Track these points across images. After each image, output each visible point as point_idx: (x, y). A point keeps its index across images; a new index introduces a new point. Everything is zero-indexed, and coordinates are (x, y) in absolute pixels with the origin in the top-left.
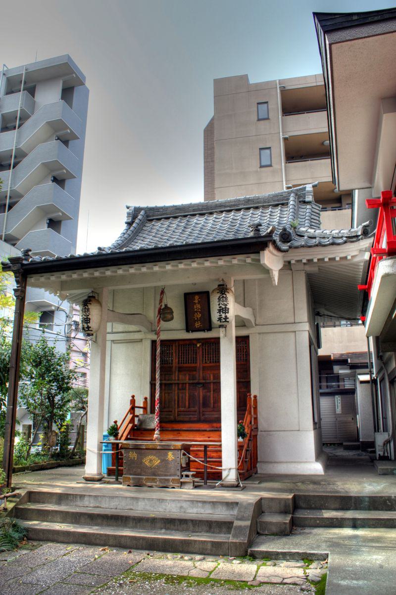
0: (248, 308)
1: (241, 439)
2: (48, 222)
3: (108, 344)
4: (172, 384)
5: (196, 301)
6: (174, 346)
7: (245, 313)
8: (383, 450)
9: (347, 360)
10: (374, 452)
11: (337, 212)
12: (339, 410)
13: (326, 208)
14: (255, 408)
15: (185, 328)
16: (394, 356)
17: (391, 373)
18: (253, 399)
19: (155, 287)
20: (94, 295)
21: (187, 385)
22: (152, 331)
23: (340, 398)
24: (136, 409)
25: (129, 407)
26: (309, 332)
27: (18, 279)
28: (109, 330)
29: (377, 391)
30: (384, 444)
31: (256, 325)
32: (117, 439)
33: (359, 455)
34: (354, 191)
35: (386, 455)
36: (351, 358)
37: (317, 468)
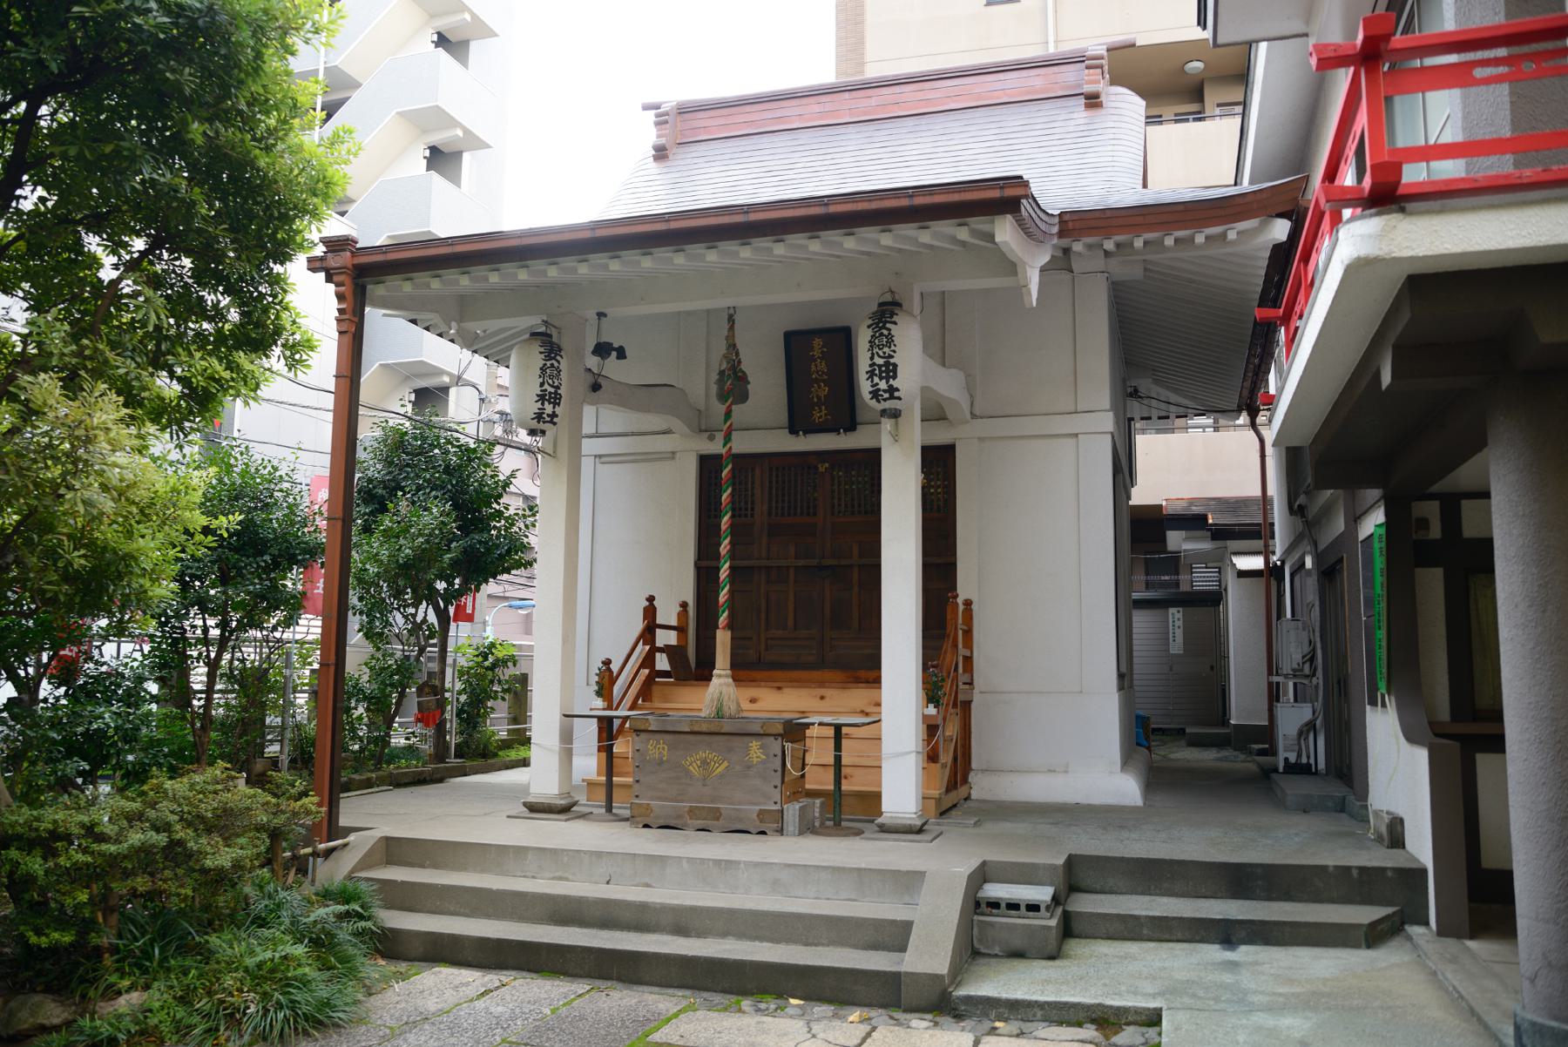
0: (953, 371)
1: (931, 710)
2: (427, 153)
3: (587, 465)
4: (752, 568)
5: (817, 353)
6: (758, 472)
7: (949, 385)
8: (1297, 748)
9: (1205, 517)
10: (1272, 751)
11: (1193, 126)
12: (1177, 646)
13: (1160, 116)
14: (968, 633)
15: (787, 425)
16: (1341, 502)
17: (1323, 551)
18: (961, 607)
19: (708, 311)
20: (549, 332)
21: (792, 571)
22: (701, 431)
23: (1180, 615)
24: (658, 631)
25: (638, 625)
26: (1113, 437)
27: (343, 288)
28: (588, 427)
29: (1281, 595)
30: (1300, 733)
31: (974, 416)
32: (610, 708)
33: (1226, 759)
34: (1254, 45)
35: (1304, 760)
36: (1214, 512)
37: (1126, 789)
